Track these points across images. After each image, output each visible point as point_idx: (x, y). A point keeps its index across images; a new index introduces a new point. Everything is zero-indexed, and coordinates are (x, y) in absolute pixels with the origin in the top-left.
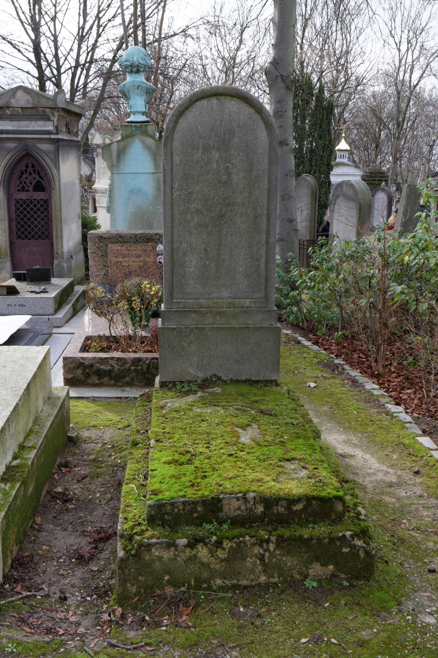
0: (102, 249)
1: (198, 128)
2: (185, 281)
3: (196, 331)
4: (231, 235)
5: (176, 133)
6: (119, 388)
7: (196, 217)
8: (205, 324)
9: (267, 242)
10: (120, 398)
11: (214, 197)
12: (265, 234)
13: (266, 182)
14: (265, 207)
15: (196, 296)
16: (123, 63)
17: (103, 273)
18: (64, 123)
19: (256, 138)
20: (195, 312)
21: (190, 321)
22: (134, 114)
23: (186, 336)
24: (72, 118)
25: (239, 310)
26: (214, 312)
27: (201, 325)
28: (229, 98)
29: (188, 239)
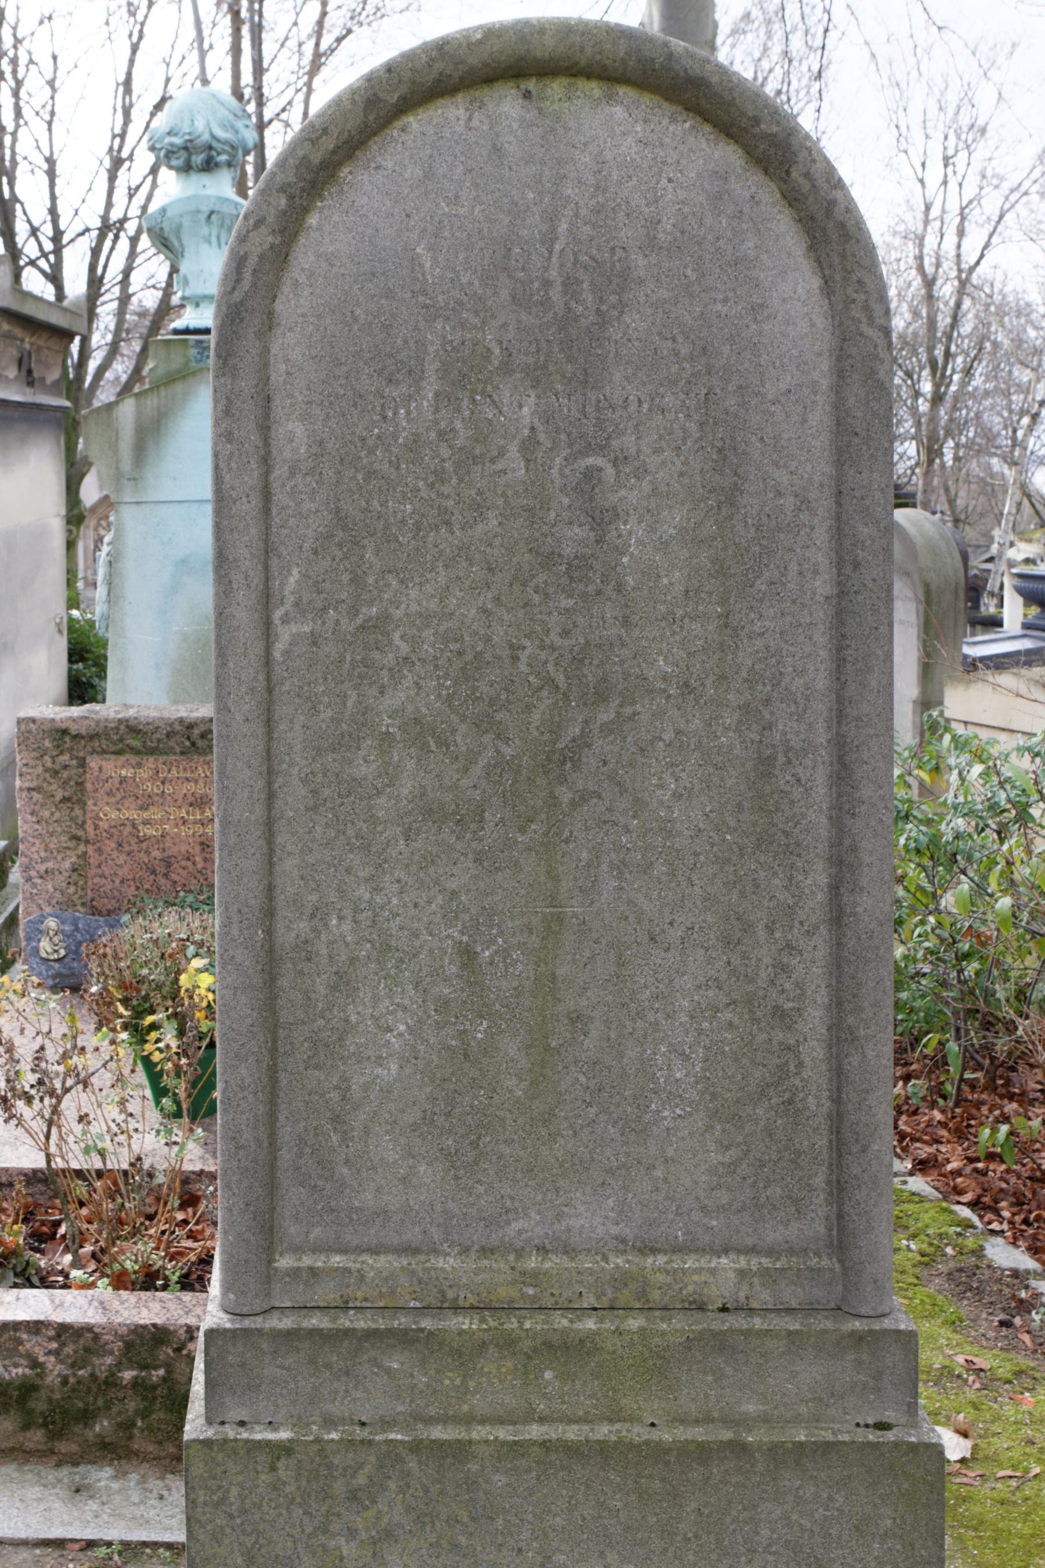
0: (65, 774)
1: (414, 261)
2: (345, 1138)
3: (412, 1464)
4: (620, 869)
5: (286, 289)
6: (65, 1471)
7: (411, 765)
8: (469, 1420)
9: (838, 917)
10: (59, 1544)
11: (515, 649)
12: (820, 865)
13: (821, 557)
14: (821, 708)
15: (413, 1235)
16: (160, 139)
17: (67, 865)
18: (14, 353)
19: (756, 309)
20: (405, 1339)
21: (377, 1398)
22: (197, 305)
23: (353, 1496)
24: (41, 342)
25: (679, 1324)
26: (526, 1345)
27: (444, 1420)
28: (594, 88)
29: (363, 892)
